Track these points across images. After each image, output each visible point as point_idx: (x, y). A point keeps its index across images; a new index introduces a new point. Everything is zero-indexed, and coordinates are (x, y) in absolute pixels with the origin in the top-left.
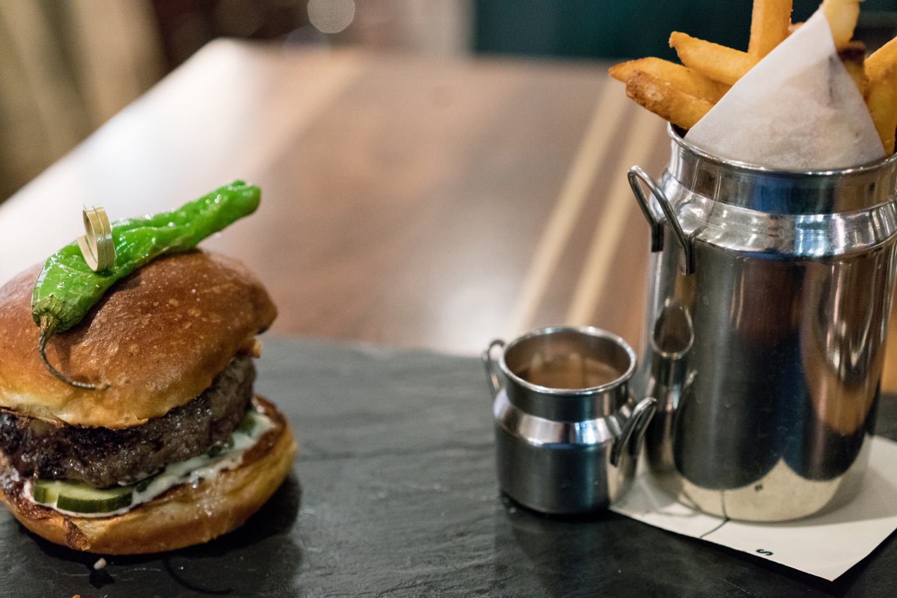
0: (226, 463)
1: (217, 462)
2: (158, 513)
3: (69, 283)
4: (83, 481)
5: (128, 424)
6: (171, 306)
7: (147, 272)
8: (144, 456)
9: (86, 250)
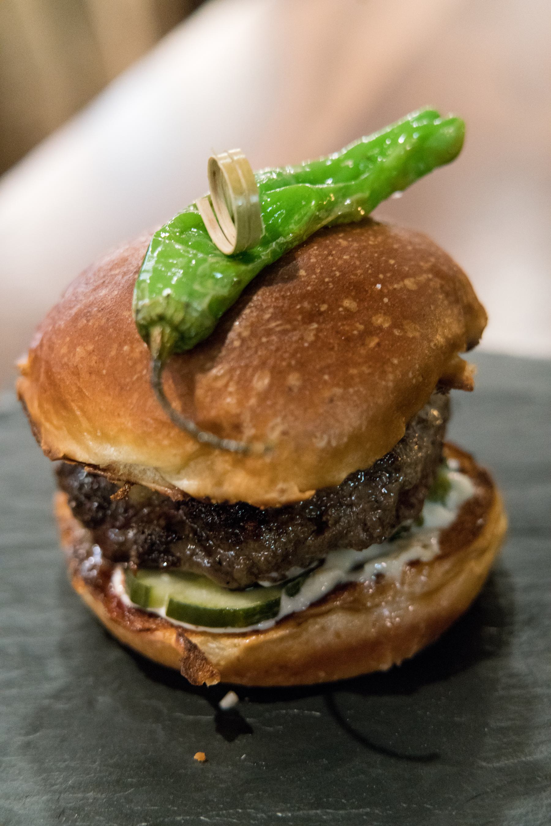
0: (416, 551)
1: (403, 548)
2: (317, 627)
3: (191, 275)
4: (204, 577)
5: (284, 498)
6: (346, 309)
7: (305, 256)
8: (299, 543)
9: (210, 221)
